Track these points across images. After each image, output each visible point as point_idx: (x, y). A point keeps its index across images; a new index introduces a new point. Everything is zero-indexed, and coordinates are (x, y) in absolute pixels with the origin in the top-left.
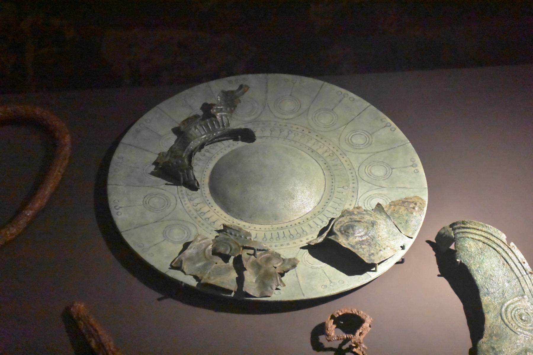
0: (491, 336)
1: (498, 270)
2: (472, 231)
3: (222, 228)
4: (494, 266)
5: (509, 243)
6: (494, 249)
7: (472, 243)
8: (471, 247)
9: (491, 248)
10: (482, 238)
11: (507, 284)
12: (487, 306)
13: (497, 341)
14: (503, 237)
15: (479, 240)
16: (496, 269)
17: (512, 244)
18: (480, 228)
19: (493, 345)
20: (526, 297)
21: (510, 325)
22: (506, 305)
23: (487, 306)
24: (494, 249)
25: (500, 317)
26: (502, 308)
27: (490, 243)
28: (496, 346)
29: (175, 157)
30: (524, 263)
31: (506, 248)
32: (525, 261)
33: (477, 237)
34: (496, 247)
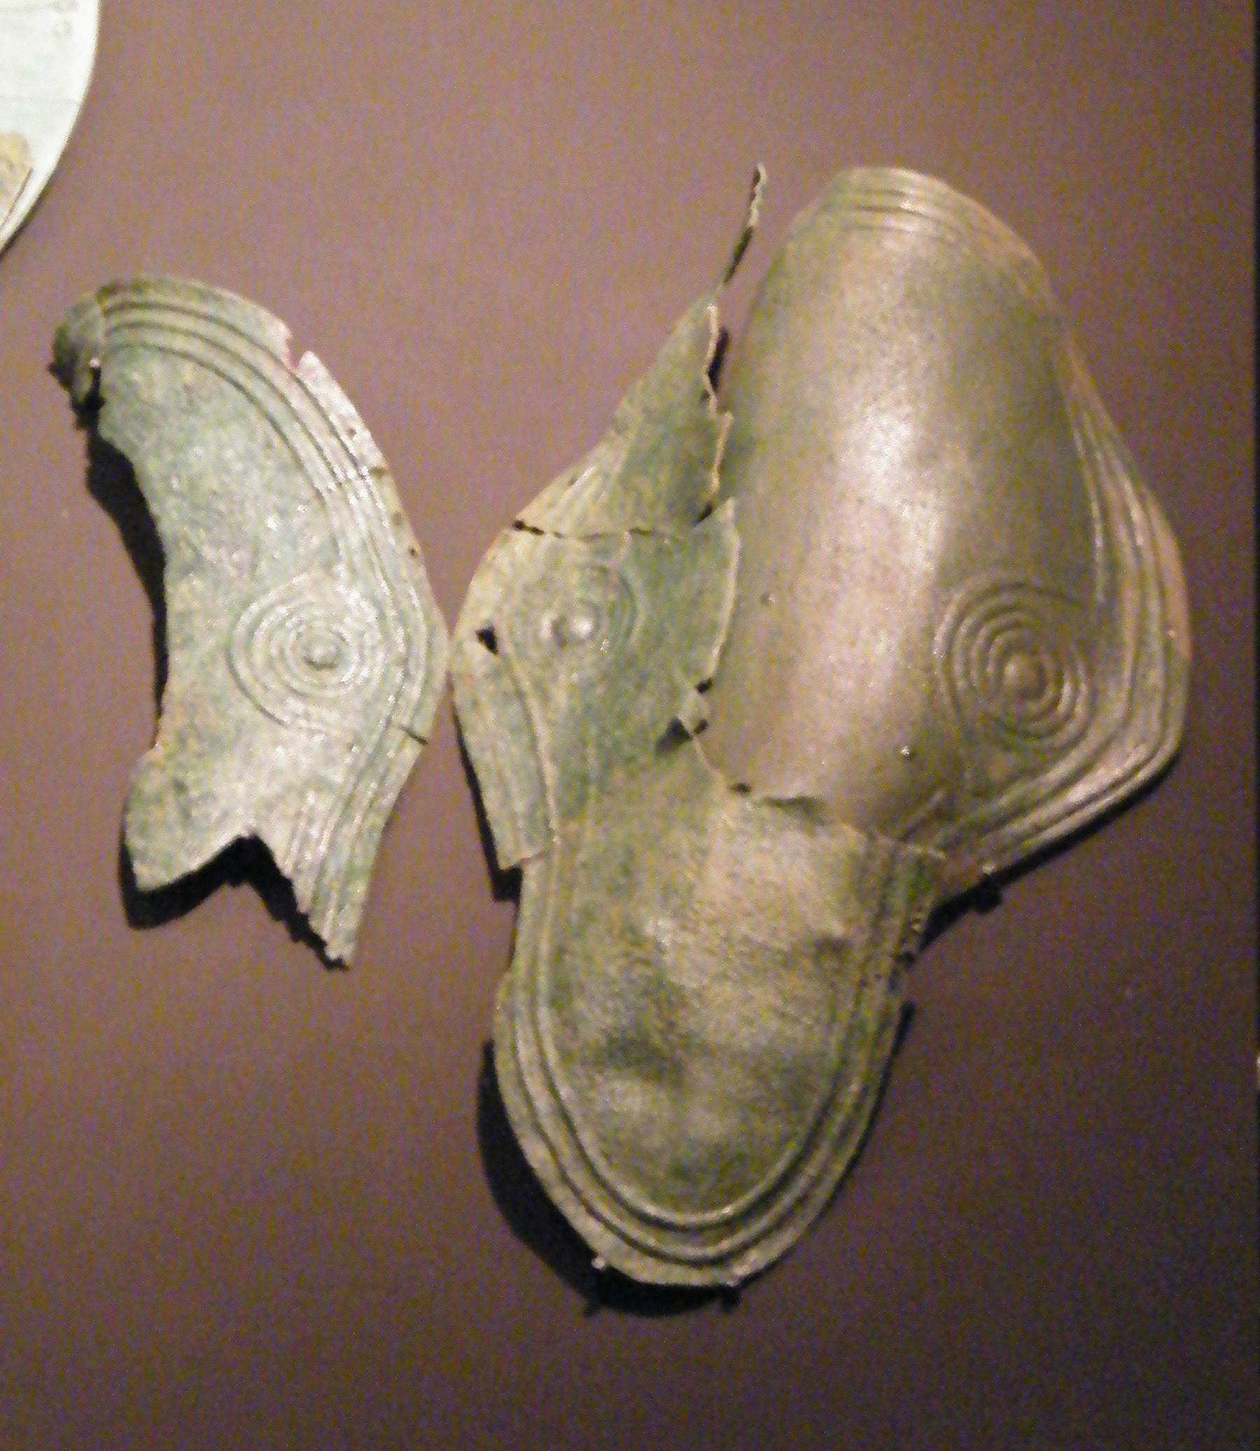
0: (182, 740)
1: (245, 472)
2: (169, 318)
3: (504, 864)
4: (229, 454)
5: (296, 358)
6: (239, 387)
7: (156, 367)
8: (150, 383)
9: (226, 386)
10: (195, 347)
11: (272, 522)
12: (186, 616)
13: (200, 755)
14: (277, 333)
15: (186, 356)
16: (238, 467)
17: (310, 359)
18: (194, 304)
19: (180, 775)
20: (341, 569)
21: (257, 690)
22: (254, 608)
23: (186, 616)
24: (239, 387)
25: (222, 661)
26: (233, 626)
27: (222, 362)
28: (190, 778)
29: (769, 851)
30: (352, 432)
31: (280, 380)
32: (358, 426)
33: (179, 343)
34: (242, 379)
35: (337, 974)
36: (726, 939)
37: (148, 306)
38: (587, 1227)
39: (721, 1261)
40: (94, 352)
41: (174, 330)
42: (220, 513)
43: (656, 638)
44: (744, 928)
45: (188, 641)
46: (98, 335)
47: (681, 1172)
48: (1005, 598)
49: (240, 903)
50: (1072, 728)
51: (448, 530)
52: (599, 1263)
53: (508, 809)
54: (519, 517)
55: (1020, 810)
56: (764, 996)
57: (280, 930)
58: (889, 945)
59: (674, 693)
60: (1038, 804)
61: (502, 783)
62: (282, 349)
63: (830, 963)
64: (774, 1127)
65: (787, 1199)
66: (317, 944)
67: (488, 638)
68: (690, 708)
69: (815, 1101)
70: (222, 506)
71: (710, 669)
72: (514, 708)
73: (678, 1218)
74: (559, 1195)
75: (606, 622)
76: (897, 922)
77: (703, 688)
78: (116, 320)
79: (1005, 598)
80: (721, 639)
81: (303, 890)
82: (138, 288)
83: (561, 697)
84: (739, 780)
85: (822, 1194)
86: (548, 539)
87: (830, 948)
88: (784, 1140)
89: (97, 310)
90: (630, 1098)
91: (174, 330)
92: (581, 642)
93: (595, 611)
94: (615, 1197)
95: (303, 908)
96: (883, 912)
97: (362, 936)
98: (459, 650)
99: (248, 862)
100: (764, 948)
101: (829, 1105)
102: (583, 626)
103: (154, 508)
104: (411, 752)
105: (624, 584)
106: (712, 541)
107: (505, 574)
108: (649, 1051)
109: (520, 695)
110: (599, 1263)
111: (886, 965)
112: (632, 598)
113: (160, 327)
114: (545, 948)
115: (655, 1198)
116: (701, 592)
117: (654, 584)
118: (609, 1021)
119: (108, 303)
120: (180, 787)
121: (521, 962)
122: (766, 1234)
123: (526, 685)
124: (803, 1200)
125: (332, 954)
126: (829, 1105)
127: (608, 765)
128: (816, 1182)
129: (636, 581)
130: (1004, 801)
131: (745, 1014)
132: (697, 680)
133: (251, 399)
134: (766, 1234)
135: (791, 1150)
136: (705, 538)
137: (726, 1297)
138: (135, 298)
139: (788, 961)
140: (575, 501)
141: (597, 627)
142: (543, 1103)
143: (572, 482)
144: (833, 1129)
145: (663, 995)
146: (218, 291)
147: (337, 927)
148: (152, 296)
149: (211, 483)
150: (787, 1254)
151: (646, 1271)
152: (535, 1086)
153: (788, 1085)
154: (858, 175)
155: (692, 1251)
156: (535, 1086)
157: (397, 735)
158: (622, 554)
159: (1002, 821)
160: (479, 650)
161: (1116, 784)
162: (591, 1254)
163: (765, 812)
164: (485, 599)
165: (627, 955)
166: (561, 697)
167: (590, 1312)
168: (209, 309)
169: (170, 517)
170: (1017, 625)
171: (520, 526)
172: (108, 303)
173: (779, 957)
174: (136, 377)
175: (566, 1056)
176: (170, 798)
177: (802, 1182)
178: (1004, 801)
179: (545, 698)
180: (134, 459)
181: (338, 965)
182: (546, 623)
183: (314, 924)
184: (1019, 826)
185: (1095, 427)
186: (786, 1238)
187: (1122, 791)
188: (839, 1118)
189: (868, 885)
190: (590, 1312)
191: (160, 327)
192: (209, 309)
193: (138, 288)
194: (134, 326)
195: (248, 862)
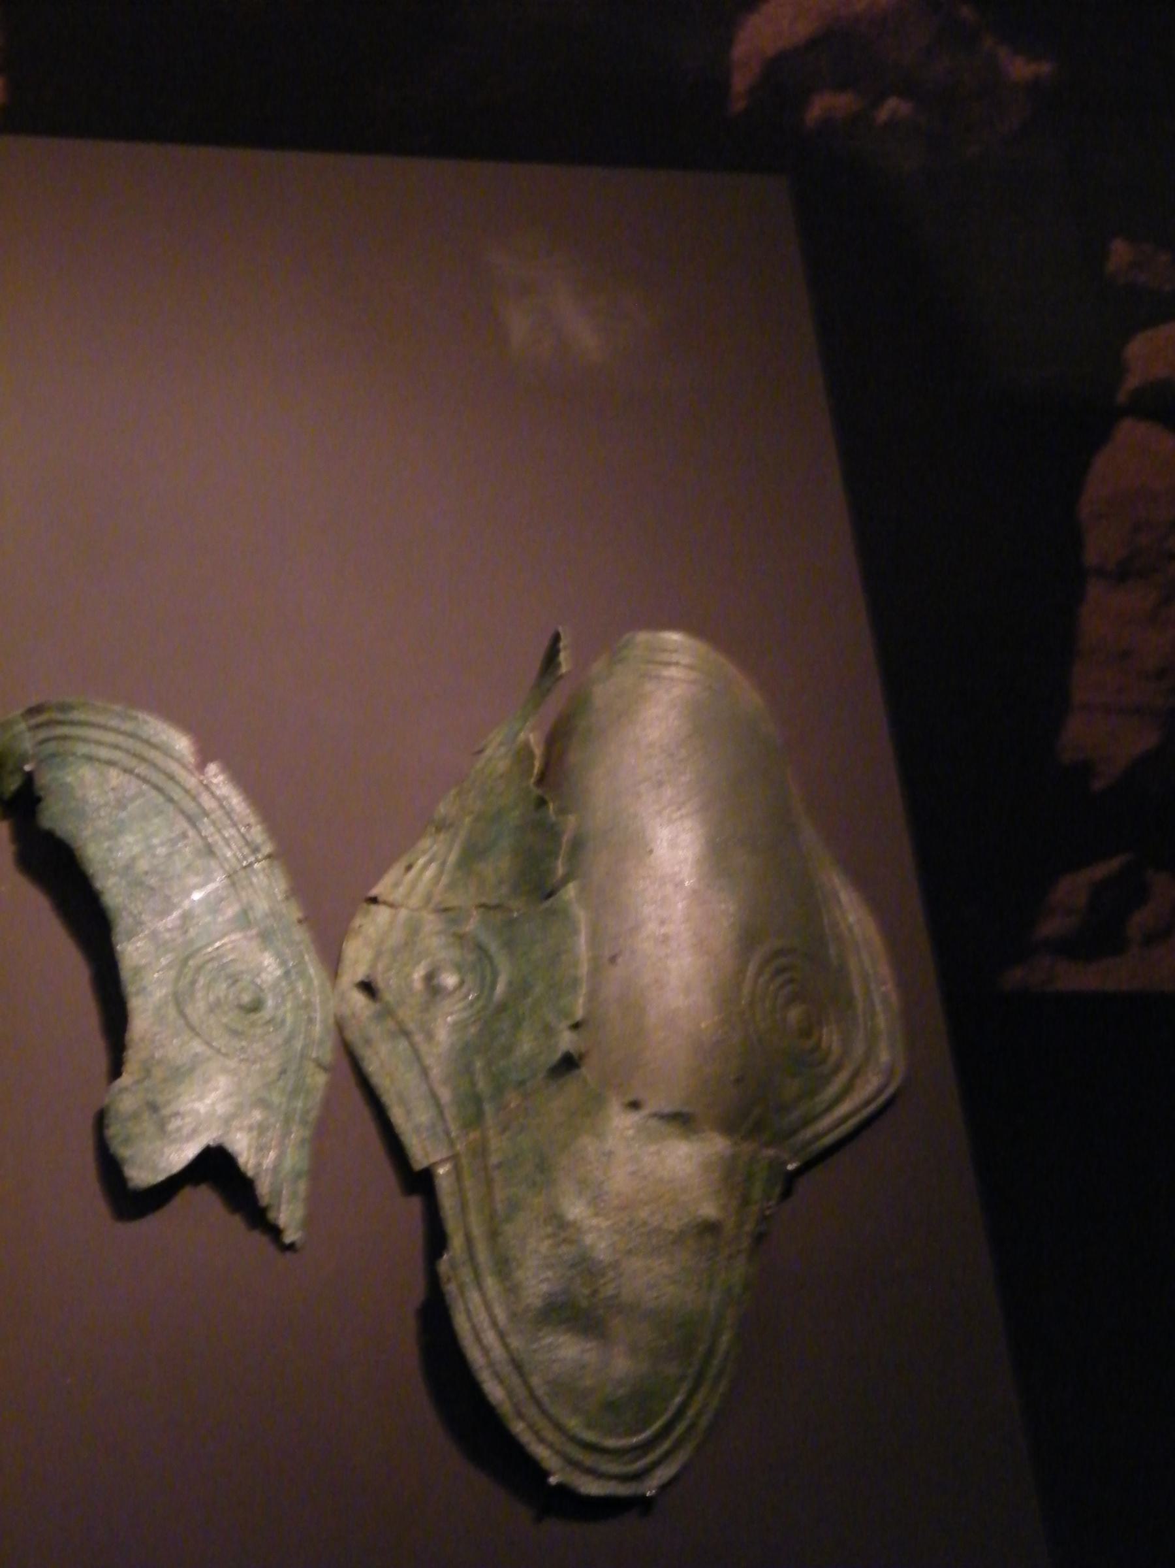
6: (159, 789)
7: (87, 772)
14: (182, 744)
15: (111, 763)
18: (114, 723)
19: (150, 1097)
23: (138, 970)
28: (160, 1099)
33: (104, 753)
35: (289, 1255)
36: (631, 1223)
37: (72, 723)
38: (541, 1452)
39: (638, 1477)
40: (24, 759)
41: (99, 743)
42: (152, 889)
43: (521, 989)
44: (643, 1214)
45: (142, 990)
46: (27, 744)
47: (610, 1406)
48: (782, 961)
49: (203, 1199)
50: (832, 1059)
51: (326, 902)
52: (553, 1480)
53: (414, 1122)
54: (374, 892)
55: (807, 1121)
56: (661, 1266)
57: (237, 1222)
58: (748, 1227)
59: (548, 1031)
60: (816, 1118)
61: (403, 1101)
62: (191, 759)
63: (709, 1240)
64: (672, 1369)
65: (680, 1428)
66: (275, 1232)
67: (368, 988)
68: (566, 1041)
69: (701, 1348)
70: (153, 881)
71: (579, 1014)
72: (403, 1044)
73: (611, 1443)
74: (518, 1428)
75: (470, 978)
76: (755, 1208)
77: (576, 1026)
78: (42, 734)
79: (782, 961)
80: (584, 990)
81: (264, 1188)
82: (64, 708)
83: (443, 1035)
84: (630, 1098)
85: (704, 1422)
86: (403, 913)
87: (710, 1228)
88: (682, 1378)
89: (22, 726)
90: (568, 1350)
91: (99, 743)
92: (451, 994)
93: (458, 968)
94: (559, 1427)
95: (264, 1201)
96: (745, 1201)
97: (309, 1222)
98: (343, 998)
99: (215, 1166)
100: (657, 1230)
101: (710, 1352)
102: (450, 980)
103: (98, 885)
104: (321, 1079)
105: (480, 948)
106: (561, 915)
107: (369, 940)
108: (573, 1312)
109: (406, 1034)
110: (553, 1480)
111: (745, 1243)
112: (490, 959)
113: (85, 740)
114: (477, 1231)
115: (589, 1426)
116: (558, 954)
117: (509, 945)
118: (545, 1287)
119: (33, 721)
120: (154, 1108)
121: (457, 1242)
122: (667, 1455)
123: (411, 1026)
124: (692, 1427)
125: (289, 1237)
126: (710, 1352)
127: (499, 1090)
128: (699, 1415)
129: (493, 947)
130: (795, 1116)
131: (654, 1280)
132: (570, 1022)
133: (170, 800)
134: (667, 1455)
135: (685, 1388)
136: (552, 912)
137: (642, 1504)
138: (60, 716)
139: (679, 1238)
140: (417, 880)
141: (462, 983)
142: (498, 1352)
143: (409, 868)
144: (712, 1372)
145: (586, 1267)
146: (134, 713)
147: (289, 1217)
148: (76, 715)
149: (143, 865)
150: (685, 1468)
151: (591, 1487)
152: (490, 1337)
153: (682, 1336)
154: (643, 637)
155: (614, 1468)
156: (490, 1337)
157: (310, 1067)
158: (471, 925)
159: (794, 1132)
160: (359, 999)
161: (867, 1103)
162: (546, 1474)
163: (654, 1123)
164: (358, 959)
165: (554, 1235)
166: (443, 1035)
167: (539, 1519)
168: (128, 726)
169: (113, 891)
170: (791, 981)
171: (374, 900)
172: (33, 721)
173: (671, 1237)
174: (69, 779)
175: (513, 1316)
176: (146, 1116)
177: (691, 1413)
178: (795, 1116)
179: (430, 1036)
180: (75, 845)
181: (291, 1247)
182: (418, 974)
183: (271, 1215)
184: (808, 1133)
185: (809, 834)
186: (682, 1457)
187: (872, 1107)
188: (716, 1362)
189: (733, 1178)
190: (539, 1519)
191: (85, 740)
192: (128, 726)
193: (64, 708)
194: (65, 738)
195: (215, 1166)
